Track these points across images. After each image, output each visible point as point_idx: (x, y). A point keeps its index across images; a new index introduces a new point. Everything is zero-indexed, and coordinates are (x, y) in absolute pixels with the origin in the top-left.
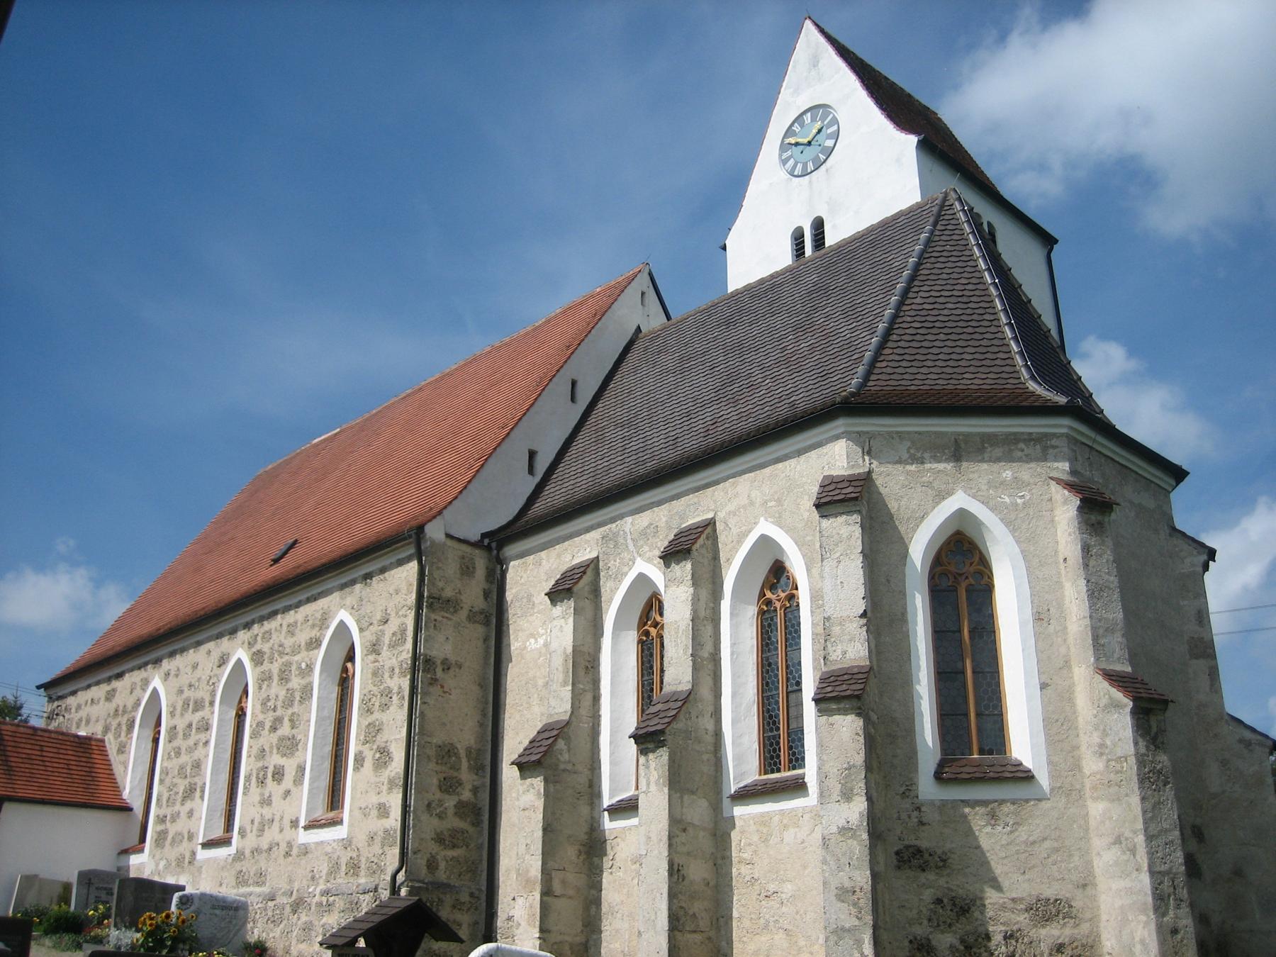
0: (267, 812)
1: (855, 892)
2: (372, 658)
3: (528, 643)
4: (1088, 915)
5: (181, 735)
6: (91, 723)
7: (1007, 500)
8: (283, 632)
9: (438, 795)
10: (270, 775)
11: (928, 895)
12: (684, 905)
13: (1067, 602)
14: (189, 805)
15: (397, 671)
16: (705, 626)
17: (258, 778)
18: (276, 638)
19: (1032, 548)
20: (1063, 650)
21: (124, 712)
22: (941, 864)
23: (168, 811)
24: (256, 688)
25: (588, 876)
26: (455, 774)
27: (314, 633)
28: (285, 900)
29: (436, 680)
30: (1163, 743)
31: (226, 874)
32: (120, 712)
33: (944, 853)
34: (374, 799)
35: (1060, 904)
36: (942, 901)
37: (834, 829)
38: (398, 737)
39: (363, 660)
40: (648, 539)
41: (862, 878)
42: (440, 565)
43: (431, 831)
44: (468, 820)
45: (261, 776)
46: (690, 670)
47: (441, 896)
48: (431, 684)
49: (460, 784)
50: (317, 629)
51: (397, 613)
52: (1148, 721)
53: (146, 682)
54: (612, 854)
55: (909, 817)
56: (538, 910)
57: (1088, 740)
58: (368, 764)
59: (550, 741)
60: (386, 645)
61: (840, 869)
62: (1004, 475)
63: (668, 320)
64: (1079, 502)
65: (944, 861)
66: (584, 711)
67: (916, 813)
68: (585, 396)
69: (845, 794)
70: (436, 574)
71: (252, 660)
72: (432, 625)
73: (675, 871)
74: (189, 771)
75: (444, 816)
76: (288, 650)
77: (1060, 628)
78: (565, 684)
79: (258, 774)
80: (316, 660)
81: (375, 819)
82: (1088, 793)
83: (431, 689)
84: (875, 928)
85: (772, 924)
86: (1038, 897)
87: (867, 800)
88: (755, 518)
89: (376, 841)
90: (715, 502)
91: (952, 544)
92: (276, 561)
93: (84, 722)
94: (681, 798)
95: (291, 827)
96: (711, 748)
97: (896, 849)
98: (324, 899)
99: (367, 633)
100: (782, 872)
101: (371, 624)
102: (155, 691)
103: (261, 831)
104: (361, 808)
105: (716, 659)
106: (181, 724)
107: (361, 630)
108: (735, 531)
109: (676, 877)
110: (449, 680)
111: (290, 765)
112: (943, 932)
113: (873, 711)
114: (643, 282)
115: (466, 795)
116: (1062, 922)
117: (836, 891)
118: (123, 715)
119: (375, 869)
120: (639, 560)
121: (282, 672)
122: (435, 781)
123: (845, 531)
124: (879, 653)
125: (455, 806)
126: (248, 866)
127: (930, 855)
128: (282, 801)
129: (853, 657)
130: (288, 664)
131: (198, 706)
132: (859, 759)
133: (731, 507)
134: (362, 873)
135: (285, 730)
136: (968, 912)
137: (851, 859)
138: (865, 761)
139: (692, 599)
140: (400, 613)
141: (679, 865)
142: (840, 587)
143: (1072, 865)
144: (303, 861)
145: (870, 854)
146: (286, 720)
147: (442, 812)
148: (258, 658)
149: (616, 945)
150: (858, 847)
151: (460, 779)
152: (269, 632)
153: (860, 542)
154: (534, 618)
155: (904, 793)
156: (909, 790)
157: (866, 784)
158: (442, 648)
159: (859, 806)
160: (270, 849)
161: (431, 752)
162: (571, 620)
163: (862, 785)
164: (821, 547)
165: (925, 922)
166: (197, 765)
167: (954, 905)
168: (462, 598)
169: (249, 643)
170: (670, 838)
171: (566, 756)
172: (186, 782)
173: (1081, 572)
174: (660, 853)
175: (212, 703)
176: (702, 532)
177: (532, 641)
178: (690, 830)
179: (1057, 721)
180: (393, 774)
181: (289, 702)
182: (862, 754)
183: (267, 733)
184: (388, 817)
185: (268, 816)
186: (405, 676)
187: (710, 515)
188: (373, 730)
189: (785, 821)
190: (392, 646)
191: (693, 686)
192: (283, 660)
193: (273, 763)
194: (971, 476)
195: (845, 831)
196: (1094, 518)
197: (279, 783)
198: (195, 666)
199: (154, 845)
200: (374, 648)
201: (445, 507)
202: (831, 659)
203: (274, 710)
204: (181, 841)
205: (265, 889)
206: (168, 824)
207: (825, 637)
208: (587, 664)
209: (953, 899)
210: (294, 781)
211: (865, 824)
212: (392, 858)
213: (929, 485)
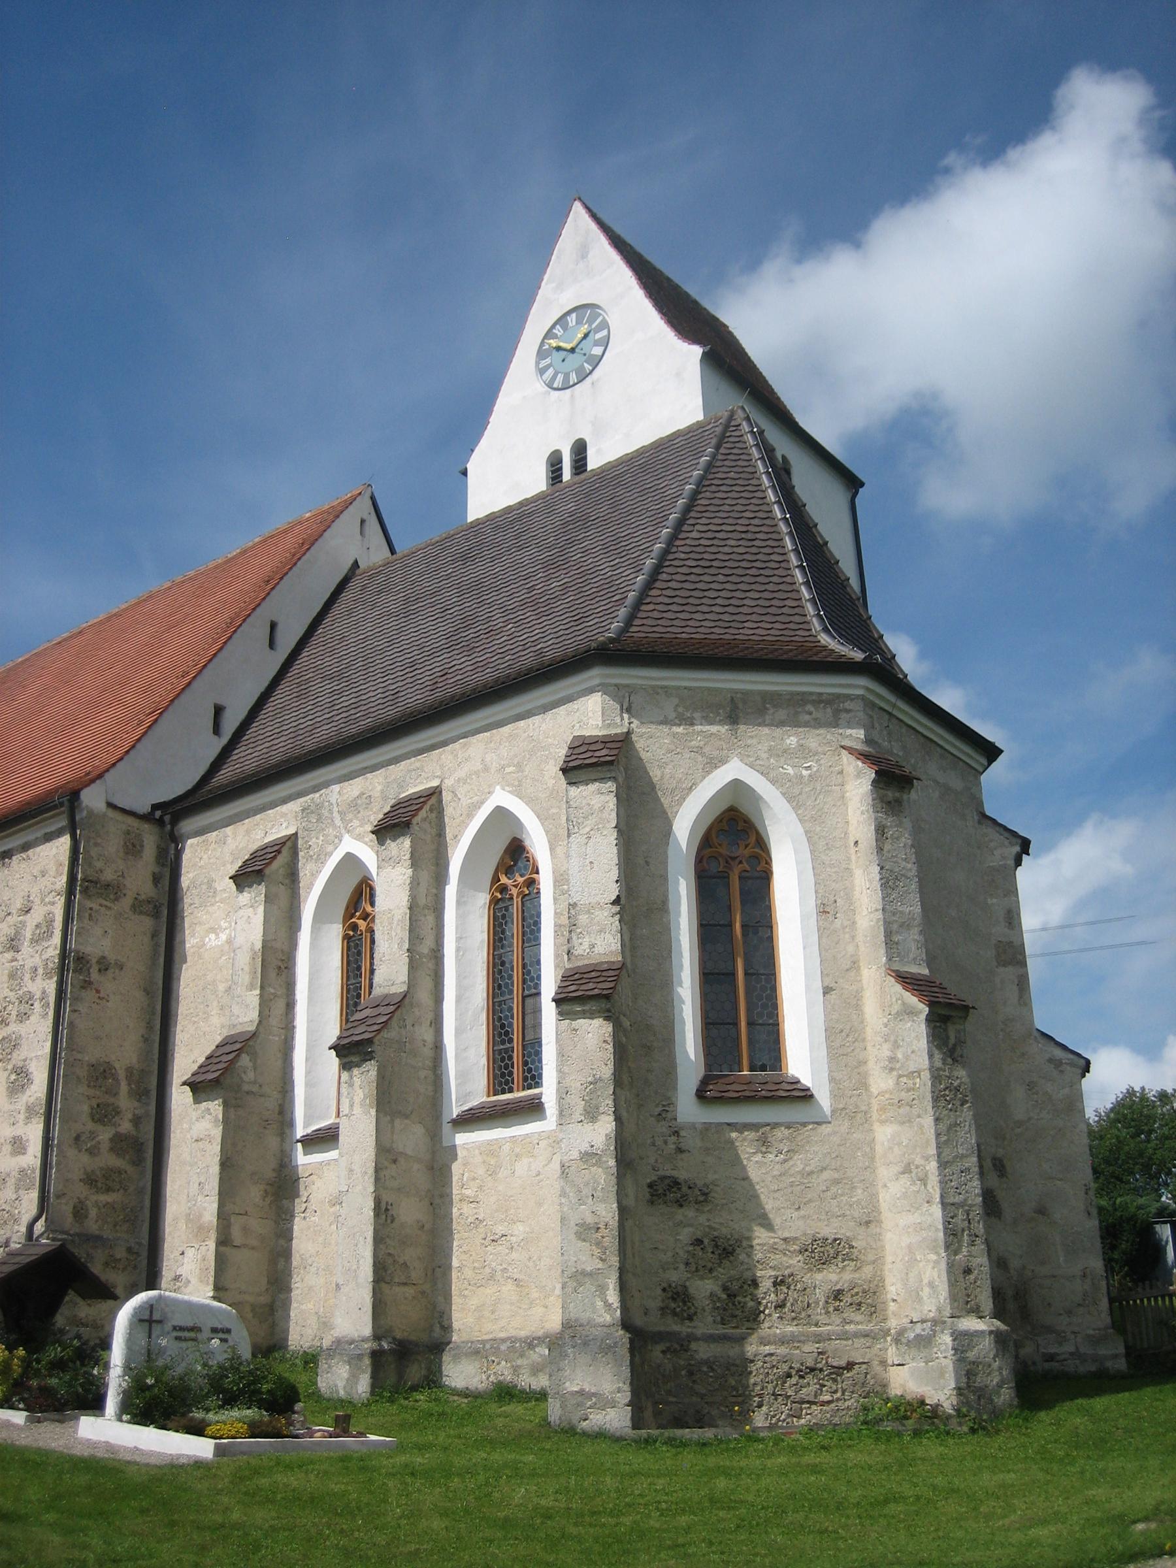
3: (207, 939)
4: (871, 1257)
7: (790, 771)
9: (90, 1126)
11: (685, 1235)
13: (857, 893)
15: (40, 971)
20: (851, 949)
22: (701, 1198)
25: (275, 1222)
26: (111, 1100)
29: (90, 983)
30: (962, 1056)
33: (706, 1185)
35: (839, 1244)
37: (575, 1154)
38: (39, 1053)
41: (608, 1212)
42: (99, 840)
44: (127, 1157)
48: (83, 987)
49: (118, 1113)
51: (42, 900)
52: (945, 1030)
54: (306, 1194)
55: (666, 1142)
56: (213, 1264)
57: (876, 1053)
62: (788, 742)
63: (392, 554)
64: (873, 775)
66: (275, 1022)
67: (674, 1139)
70: (94, 852)
72: (87, 915)
73: (382, 1211)
78: (251, 987)
81: (8, 1156)
82: (875, 1116)
83: (83, 994)
84: (622, 1271)
87: (615, 1120)
88: (490, 786)
89: (8, 1184)
90: (442, 767)
94: (392, 1121)
100: (512, 1211)
101: (9, 914)
105: (437, 955)
108: (465, 802)
109: (384, 1217)
110: (107, 984)
112: (702, 1278)
114: (363, 507)
115: (126, 1126)
116: (840, 1265)
120: (347, 838)
122: (86, 1108)
124: (633, 948)
125: (111, 1140)
127: (690, 1188)
133: (461, 773)
136: (732, 1253)
137: (595, 1189)
138: (614, 1074)
140: (47, 900)
141: (387, 1203)
145: (618, 1184)
150: (604, 1175)
151: (118, 1107)
153: (614, 815)
155: (660, 1114)
156: (666, 1112)
159: (606, 1126)
161: (82, 1072)
162: (261, 909)
163: (610, 1102)
165: (682, 1267)
167: (717, 1246)
170: (377, 1170)
171: (251, 1075)
173: (874, 857)
174: (365, 1189)
176: (424, 803)
177: (212, 936)
178: (402, 1160)
180: (32, 1100)
182: (611, 1066)
184: (24, 1154)
186: (51, 978)
187: (435, 783)
189: (517, 1150)
190: (35, 941)
191: (409, 988)
194: (749, 742)
195: (588, 1157)
196: (891, 794)
202: (576, 953)
207: (569, 928)
208: (280, 964)
209: (714, 1240)
213: (699, 750)
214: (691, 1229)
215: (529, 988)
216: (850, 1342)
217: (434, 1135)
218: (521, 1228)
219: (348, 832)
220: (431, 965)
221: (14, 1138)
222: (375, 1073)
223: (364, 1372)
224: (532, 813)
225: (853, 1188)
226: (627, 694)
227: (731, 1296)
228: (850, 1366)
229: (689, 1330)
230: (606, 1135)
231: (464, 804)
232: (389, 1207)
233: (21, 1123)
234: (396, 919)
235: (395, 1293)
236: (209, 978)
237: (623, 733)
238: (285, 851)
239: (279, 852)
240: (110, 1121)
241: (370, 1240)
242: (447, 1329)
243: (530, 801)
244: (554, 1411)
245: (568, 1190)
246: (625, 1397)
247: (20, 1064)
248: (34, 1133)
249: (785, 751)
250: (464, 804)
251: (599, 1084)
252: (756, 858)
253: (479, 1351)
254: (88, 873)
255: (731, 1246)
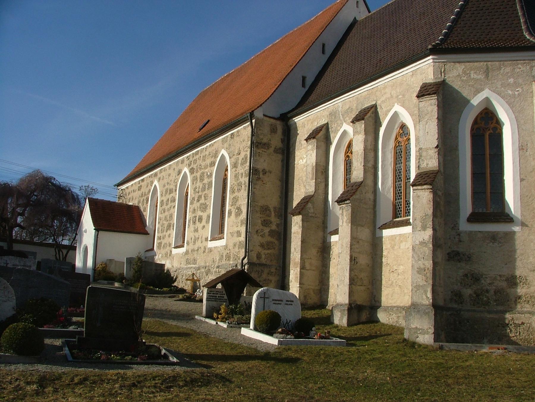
0: (197, 235)
1: (425, 270)
2: (234, 169)
3: (299, 162)
5: (165, 204)
6: (134, 200)
7: (510, 92)
8: (201, 160)
9: (261, 227)
10: (197, 219)
11: (461, 273)
12: (357, 274)
14: (169, 232)
15: (244, 175)
16: (370, 153)
17: (193, 221)
18: (199, 162)
19: (521, 115)
21: (145, 195)
22: (468, 259)
23: (161, 235)
24: (192, 183)
25: (322, 262)
26: (269, 218)
27: (213, 159)
28: (203, 270)
29: (260, 178)
31: (183, 260)
32: (143, 195)
33: (469, 254)
34: (236, 229)
35: (522, 278)
36: (467, 275)
37: (418, 243)
38: (244, 203)
39: (231, 170)
40: (348, 114)
41: (429, 264)
42: (261, 128)
43: (258, 242)
44: (275, 238)
45: (194, 220)
46: (362, 172)
47: (262, 269)
49: (271, 223)
50: (214, 158)
51: (244, 150)
53: (152, 182)
55: (455, 238)
56: (299, 276)
58: (233, 214)
59: (305, 204)
60: (240, 164)
61: (419, 260)
62: (510, 81)
63: (369, 13)
65: (469, 258)
67: (457, 237)
68: (329, 52)
69: (423, 227)
70: (259, 132)
71: (190, 172)
72: (258, 155)
74: (168, 218)
75: (264, 236)
76: (203, 167)
77: (532, 153)
78: (312, 179)
79: (193, 219)
80: (214, 170)
81: (236, 237)
84: (433, 286)
85: (394, 283)
86: (512, 275)
87: (433, 230)
88: (393, 103)
89: (236, 246)
91: (483, 114)
92: (200, 129)
93: (131, 199)
94: (357, 228)
95: (205, 240)
96: (372, 207)
97: (447, 252)
98: (217, 270)
99: (232, 159)
100: (399, 261)
102: (155, 186)
103: (194, 242)
104: (231, 233)
105: (375, 168)
106: (165, 199)
107: (230, 158)
108: (385, 110)
109: (353, 262)
111: (204, 215)
113: (439, 190)
115: (274, 227)
116: (522, 286)
117: (417, 269)
118: (144, 196)
119: (236, 258)
120: (344, 124)
121: (201, 176)
122: (260, 221)
123: (430, 109)
124: (444, 165)
126: (190, 257)
128: (202, 230)
129: (431, 166)
130: (203, 173)
131: (171, 191)
132: (430, 212)
133: (383, 99)
134: (231, 260)
135: (202, 201)
138: (433, 213)
139: (364, 141)
140: (245, 150)
141: (355, 258)
142: (427, 134)
143: (529, 261)
144: (210, 255)
146: (203, 196)
147: (263, 234)
148: (192, 171)
149: (332, 291)
150: (428, 250)
152: (196, 160)
154: (302, 150)
156: (455, 226)
157: (433, 223)
158: (262, 165)
159: (429, 232)
160: (198, 250)
161: (258, 209)
162: (315, 151)
163: (431, 223)
164: (419, 116)
165: (459, 284)
166: (171, 216)
168: (271, 142)
169: (189, 165)
172: (168, 223)
174: (347, 252)
175: (176, 190)
176: (369, 111)
177: (301, 161)
178: (361, 242)
179: (527, 196)
181: (204, 189)
182: (432, 210)
183: (196, 202)
184: (240, 237)
185: (197, 236)
186: (247, 177)
187: (374, 103)
188: (235, 200)
190: (242, 164)
191: (364, 179)
192: (201, 171)
193: (198, 215)
197: (201, 223)
198: (169, 175)
199: (157, 248)
200: (235, 166)
201: (263, 103)
202: (421, 167)
203: (198, 193)
204: (167, 246)
205: (197, 266)
206: (162, 240)
207: (419, 157)
208: (322, 170)
209: (472, 275)
210: (206, 222)
211: (431, 240)
212: (242, 254)
214: (463, 270)
215: (408, 180)
216: (523, 315)
217: (374, 233)
218: (402, 267)
219: (345, 122)
220: (372, 171)
221: (238, 231)
222: (350, 211)
223: (345, 315)
224: (408, 114)
225: (529, 257)
226: (443, 65)
227: (478, 296)
228: (523, 323)
229: (460, 307)
230: (429, 236)
231: (384, 110)
232: (355, 259)
233: (239, 226)
234: (359, 154)
235: (358, 288)
236: (300, 175)
237: (441, 81)
238: (324, 130)
239: (321, 130)
240: (268, 225)
241: (348, 270)
242: (380, 302)
243: (407, 109)
244: (406, 336)
245: (414, 255)
246: (432, 331)
247: (239, 206)
248: (243, 229)
249: (508, 84)
250: (384, 110)
251: (427, 217)
252: (495, 129)
253: (389, 309)
254: (258, 140)
255: (478, 277)
